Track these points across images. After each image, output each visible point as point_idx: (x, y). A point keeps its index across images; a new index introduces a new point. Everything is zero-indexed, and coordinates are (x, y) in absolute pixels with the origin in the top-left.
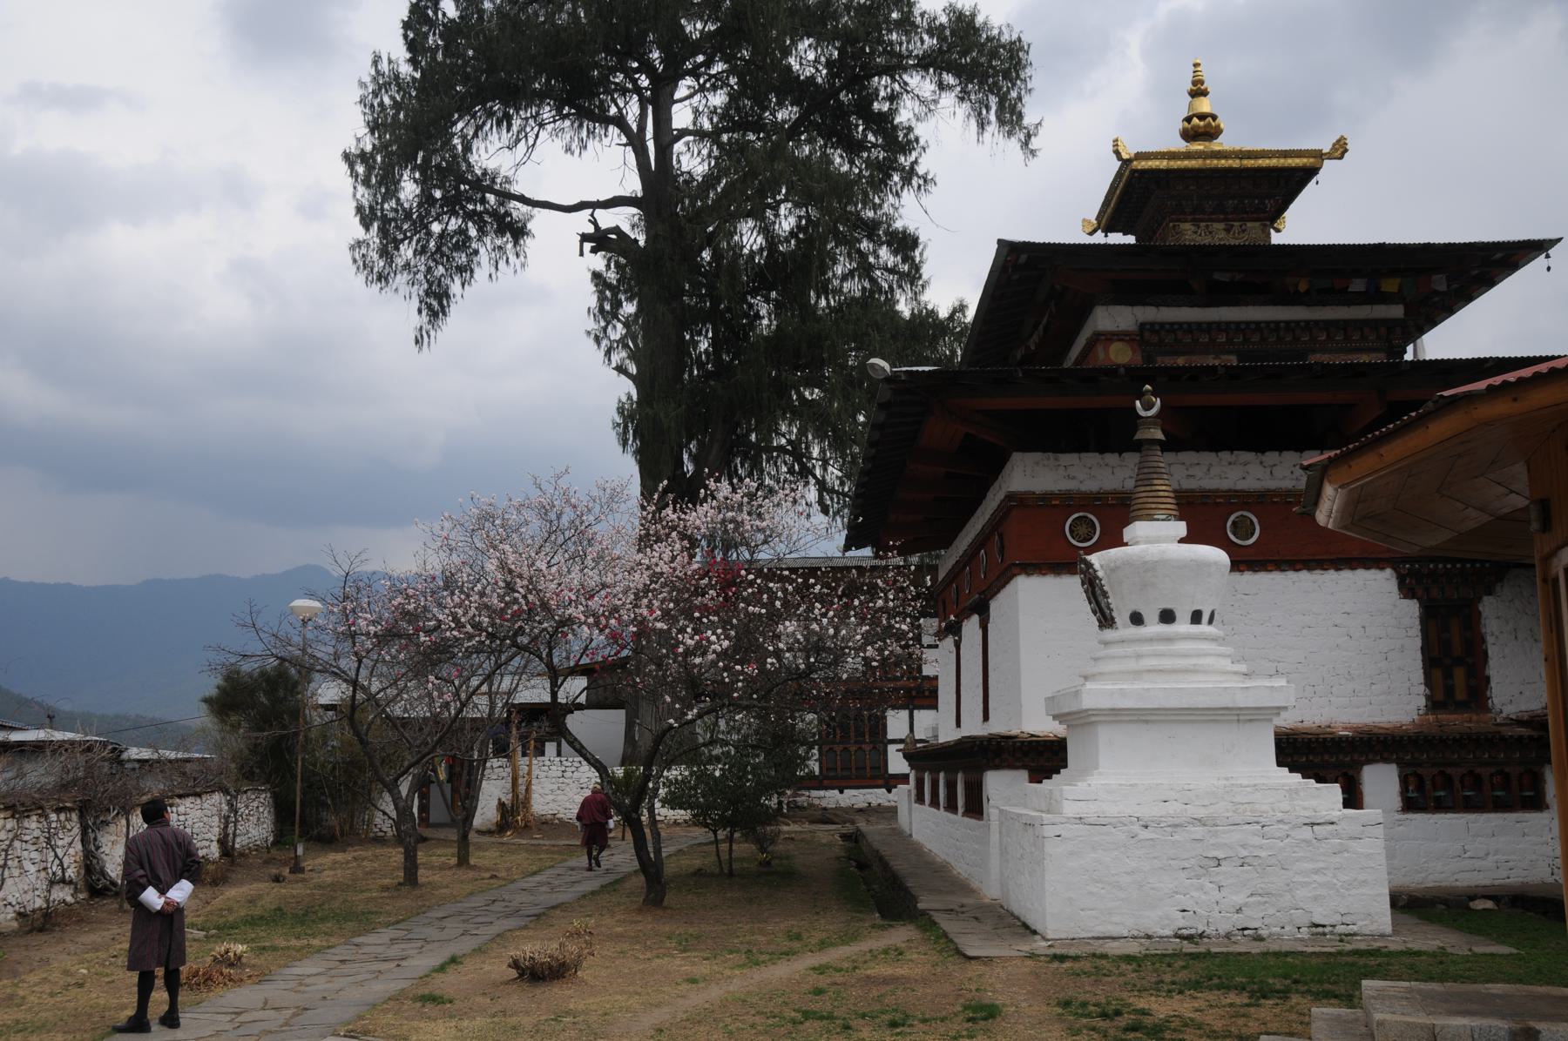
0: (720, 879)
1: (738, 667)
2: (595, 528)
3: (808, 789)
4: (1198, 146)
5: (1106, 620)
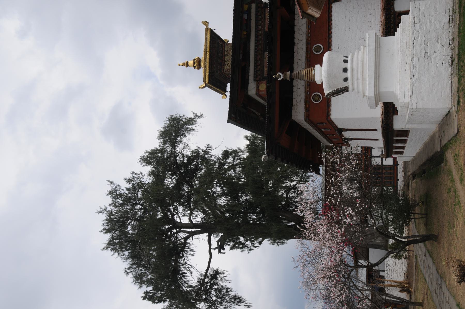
0: (427, 218)
1: (358, 205)
2: (311, 250)
3: (397, 190)
4: (203, 64)
5: (346, 89)
